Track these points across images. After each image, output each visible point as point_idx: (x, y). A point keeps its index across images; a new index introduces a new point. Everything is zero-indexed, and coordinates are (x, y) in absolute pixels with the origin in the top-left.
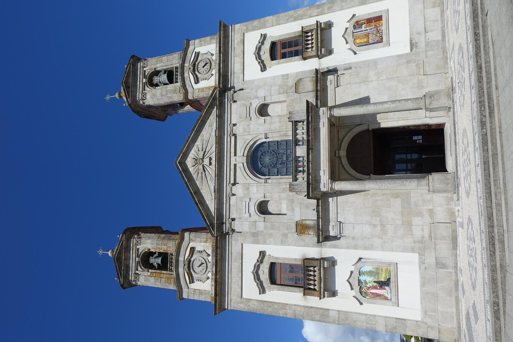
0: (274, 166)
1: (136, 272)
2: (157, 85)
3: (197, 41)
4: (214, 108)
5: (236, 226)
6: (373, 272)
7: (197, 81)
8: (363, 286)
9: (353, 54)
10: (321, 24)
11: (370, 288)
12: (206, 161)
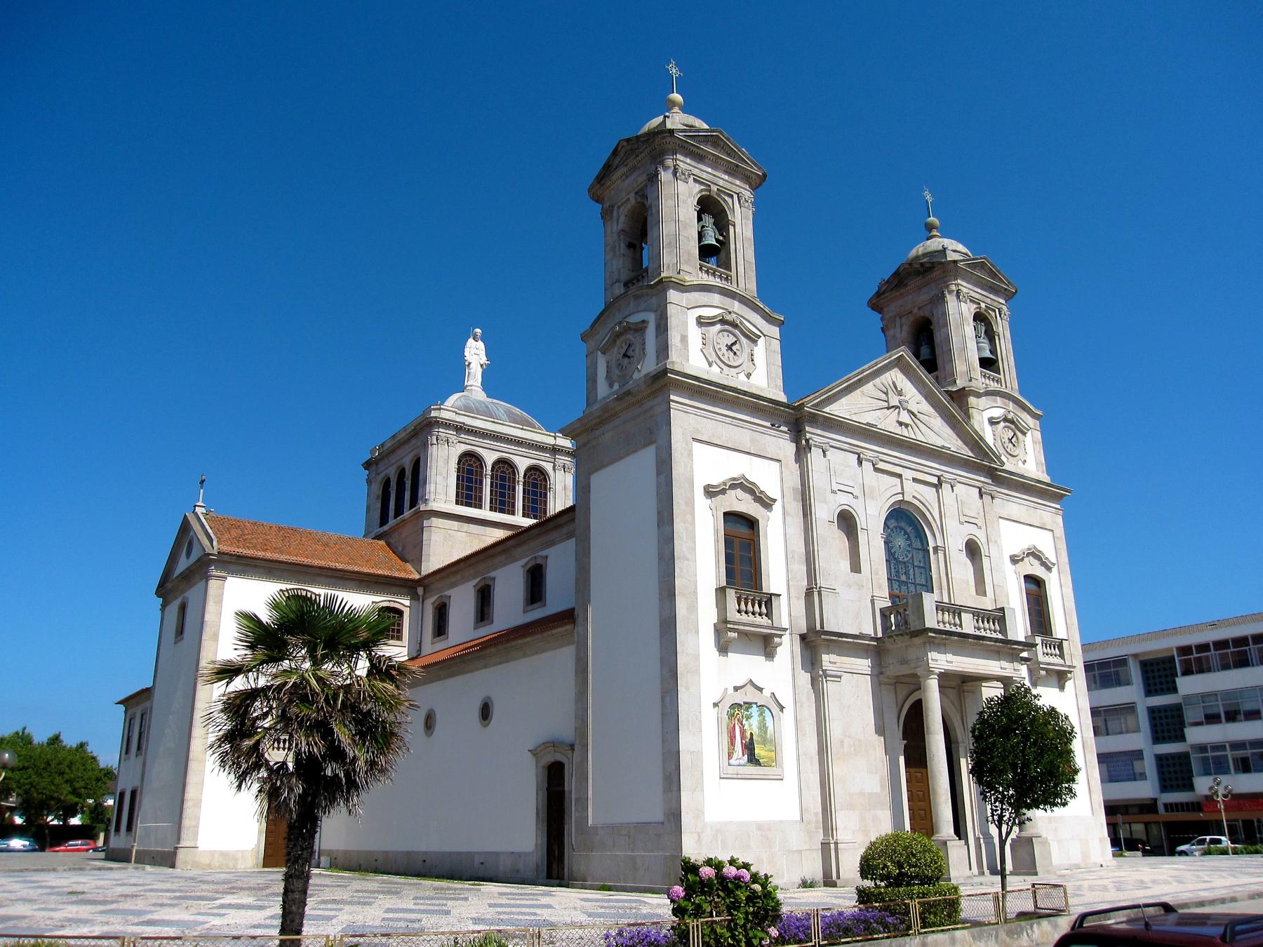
4: (972, 451)
6: (766, 733)
7: (701, 322)
9: (716, 700)
10: (780, 636)
11: (742, 724)
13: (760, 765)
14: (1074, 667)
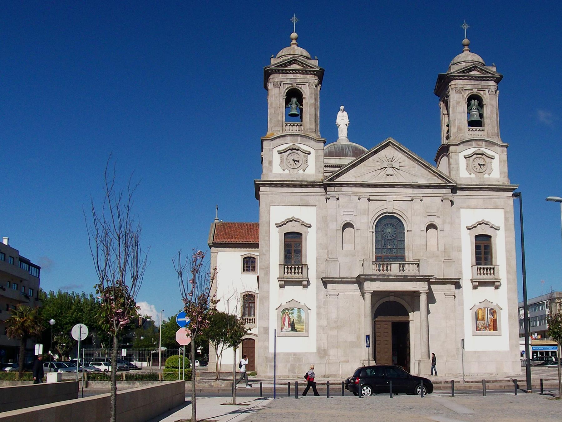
0: (383, 237)
1: (282, 83)
2: (469, 105)
3: (505, 157)
5: (332, 202)
6: (301, 319)
8: (289, 311)
11: (289, 316)
12: (390, 171)
13: (297, 331)
14: (500, 279)
